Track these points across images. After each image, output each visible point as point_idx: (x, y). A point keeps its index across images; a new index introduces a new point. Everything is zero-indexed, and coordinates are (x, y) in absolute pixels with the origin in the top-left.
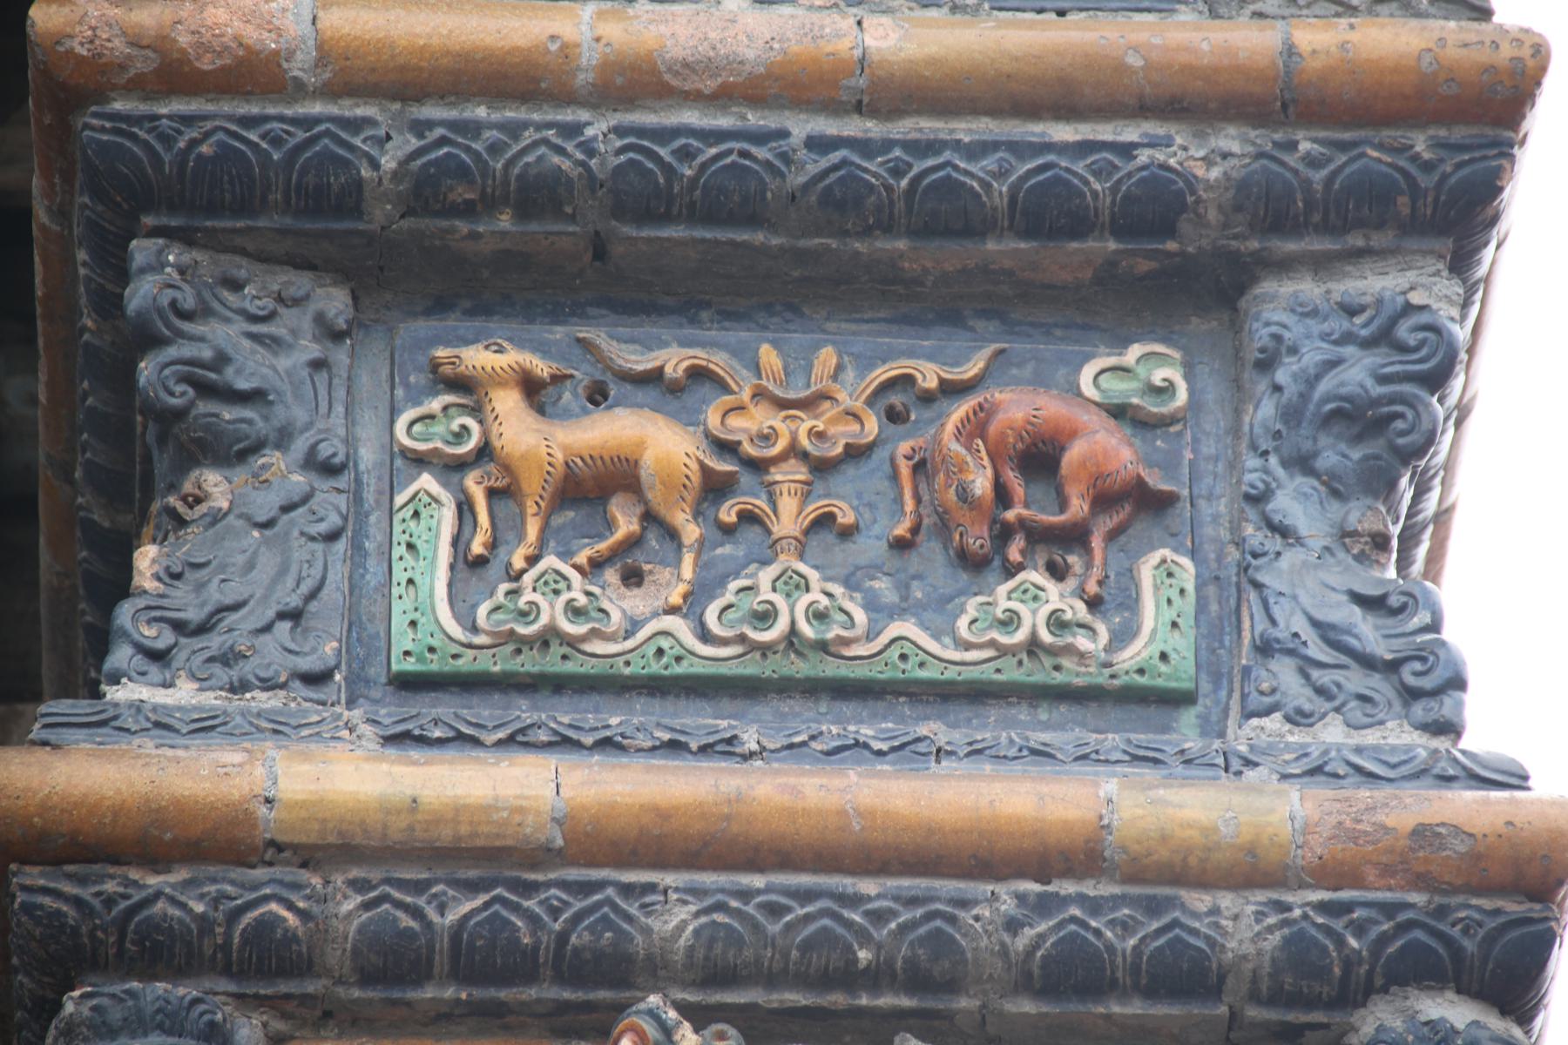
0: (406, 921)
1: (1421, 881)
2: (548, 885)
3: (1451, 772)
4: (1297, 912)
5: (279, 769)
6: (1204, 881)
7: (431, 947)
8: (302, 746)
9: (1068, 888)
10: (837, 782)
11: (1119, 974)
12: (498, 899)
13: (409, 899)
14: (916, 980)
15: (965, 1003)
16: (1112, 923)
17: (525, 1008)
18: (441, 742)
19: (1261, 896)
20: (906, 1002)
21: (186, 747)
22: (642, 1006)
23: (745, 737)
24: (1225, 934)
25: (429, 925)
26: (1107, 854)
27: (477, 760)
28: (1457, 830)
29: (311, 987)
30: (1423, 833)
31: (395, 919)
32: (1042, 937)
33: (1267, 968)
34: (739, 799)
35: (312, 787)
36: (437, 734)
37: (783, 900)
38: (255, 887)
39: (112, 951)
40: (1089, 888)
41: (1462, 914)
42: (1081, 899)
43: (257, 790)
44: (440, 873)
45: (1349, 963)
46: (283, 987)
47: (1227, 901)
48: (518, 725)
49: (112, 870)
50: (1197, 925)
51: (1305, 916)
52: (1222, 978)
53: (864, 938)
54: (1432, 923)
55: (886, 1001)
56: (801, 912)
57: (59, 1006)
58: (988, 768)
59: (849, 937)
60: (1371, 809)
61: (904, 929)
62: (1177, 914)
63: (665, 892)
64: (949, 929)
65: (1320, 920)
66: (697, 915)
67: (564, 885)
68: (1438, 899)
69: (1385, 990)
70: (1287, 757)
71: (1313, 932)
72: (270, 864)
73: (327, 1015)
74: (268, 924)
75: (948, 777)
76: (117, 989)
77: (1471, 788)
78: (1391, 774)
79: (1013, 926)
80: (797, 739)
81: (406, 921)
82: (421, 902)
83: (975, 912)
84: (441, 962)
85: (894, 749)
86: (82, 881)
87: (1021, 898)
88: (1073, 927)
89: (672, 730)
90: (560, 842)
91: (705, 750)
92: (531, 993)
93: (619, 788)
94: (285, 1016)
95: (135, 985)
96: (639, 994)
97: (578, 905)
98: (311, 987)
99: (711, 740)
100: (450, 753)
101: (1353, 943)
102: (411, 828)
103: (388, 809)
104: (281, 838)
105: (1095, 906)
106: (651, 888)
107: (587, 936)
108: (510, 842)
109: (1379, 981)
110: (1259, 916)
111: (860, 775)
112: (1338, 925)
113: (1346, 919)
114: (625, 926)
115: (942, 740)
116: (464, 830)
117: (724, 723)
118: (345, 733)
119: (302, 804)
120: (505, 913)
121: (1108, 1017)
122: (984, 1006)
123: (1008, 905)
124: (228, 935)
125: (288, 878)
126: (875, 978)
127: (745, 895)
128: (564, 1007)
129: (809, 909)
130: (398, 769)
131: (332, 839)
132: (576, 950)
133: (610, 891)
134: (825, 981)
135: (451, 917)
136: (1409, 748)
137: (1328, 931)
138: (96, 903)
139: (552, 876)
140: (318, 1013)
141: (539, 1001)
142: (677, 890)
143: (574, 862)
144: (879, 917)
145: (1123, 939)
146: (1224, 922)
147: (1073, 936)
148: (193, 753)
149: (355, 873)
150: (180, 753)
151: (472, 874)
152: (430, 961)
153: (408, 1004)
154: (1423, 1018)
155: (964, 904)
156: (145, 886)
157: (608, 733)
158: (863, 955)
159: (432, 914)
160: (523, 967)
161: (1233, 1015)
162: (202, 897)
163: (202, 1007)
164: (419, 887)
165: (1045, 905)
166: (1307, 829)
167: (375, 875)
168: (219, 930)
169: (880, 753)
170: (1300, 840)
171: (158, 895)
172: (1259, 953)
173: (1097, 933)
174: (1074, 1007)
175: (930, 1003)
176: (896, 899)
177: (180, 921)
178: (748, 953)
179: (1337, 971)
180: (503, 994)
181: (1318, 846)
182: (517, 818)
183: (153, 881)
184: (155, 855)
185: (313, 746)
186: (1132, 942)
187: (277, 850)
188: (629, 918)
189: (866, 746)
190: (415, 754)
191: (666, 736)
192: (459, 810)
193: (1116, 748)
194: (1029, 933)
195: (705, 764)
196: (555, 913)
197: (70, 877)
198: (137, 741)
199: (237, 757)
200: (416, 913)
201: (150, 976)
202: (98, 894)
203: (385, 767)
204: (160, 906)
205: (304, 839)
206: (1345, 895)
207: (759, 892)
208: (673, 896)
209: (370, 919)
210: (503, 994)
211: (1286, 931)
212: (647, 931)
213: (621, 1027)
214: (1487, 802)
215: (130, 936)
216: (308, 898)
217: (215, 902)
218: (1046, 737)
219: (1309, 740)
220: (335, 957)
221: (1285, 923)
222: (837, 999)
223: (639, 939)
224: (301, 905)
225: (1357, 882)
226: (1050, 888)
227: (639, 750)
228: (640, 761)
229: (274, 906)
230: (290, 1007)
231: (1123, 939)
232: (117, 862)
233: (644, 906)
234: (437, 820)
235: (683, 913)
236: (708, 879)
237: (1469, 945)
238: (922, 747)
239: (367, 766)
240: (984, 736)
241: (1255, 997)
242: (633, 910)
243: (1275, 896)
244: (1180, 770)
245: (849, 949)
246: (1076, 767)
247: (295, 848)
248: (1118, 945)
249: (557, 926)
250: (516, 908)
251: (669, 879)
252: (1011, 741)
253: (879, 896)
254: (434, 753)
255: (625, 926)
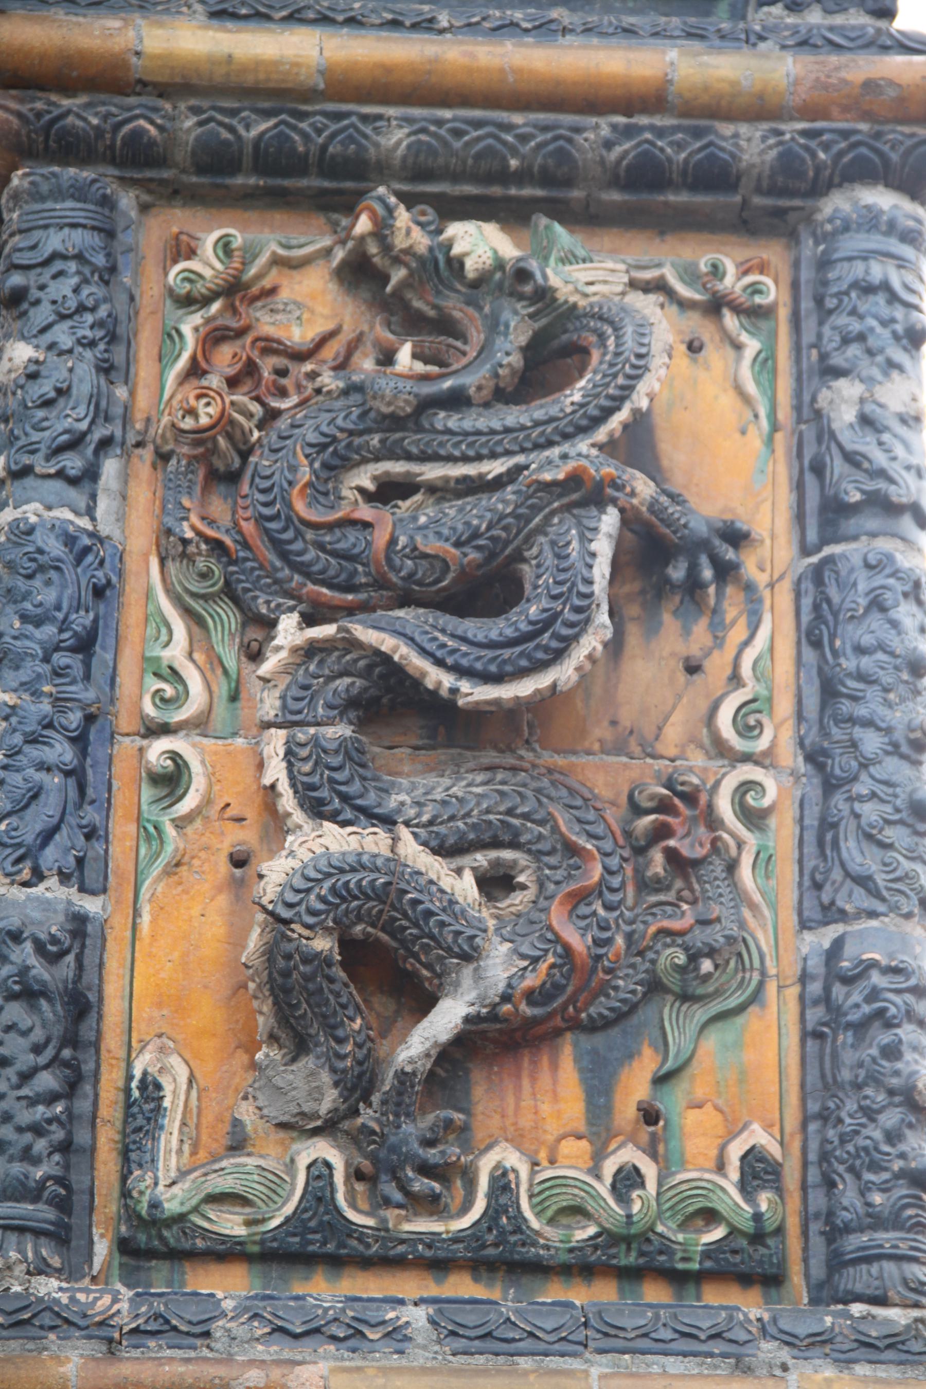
0: (225, 135)
1: (866, 116)
2: (315, 113)
3: (889, 43)
4: (788, 137)
5: (144, 32)
6: (729, 117)
7: (241, 152)
8: (157, 17)
9: (644, 120)
10: (499, 50)
11: (674, 176)
12: (283, 122)
13: (227, 120)
14: (546, 179)
15: (576, 194)
16: (671, 144)
17: (299, 192)
18: (246, 17)
19: (765, 126)
20: (539, 193)
21: (85, 16)
22: (374, 194)
23: (440, 18)
24: (741, 149)
25: (239, 137)
26: (670, 98)
27: (270, 30)
28: (891, 83)
29: (166, 174)
30: (870, 85)
31: (218, 134)
32: (626, 153)
33: (767, 172)
34: (436, 60)
35: (165, 45)
36: (244, 11)
37: (463, 126)
38: (130, 109)
39: (41, 147)
40: (659, 121)
41: (891, 137)
42: (652, 128)
43: (130, 46)
44: (246, 104)
45: (818, 169)
46: (149, 174)
47: (744, 129)
48: (295, 7)
49: (40, 94)
50: (724, 144)
51: (793, 139)
52: (738, 178)
53: (514, 152)
54: (871, 142)
55: (527, 192)
56: (475, 134)
57: (8, 180)
58: (595, 41)
59: (504, 150)
60: (837, 69)
61: (540, 146)
62: (712, 137)
63: (389, 120)
64: (568, 147)
65: (802, 141)
66: (409, 135)
67: (325, 114)
68: (877, 127)
69: (840, 185)
70: (786, 33)
71: (797, 149)
72: (139, 94)
73: (176, 192)
74: (138, 134)
75: (570, 47)
76: (45, 170)
77: (900, 53)
78: (851, 45)
79: (608, 145)
80: (474, 20)
81: (225, 135)
82: (234, 122)
83: (585, 135)
84: (247, 161)
85: (535, 28)
86: (22, 101)
87: (614, 127)
88: (646, 146)
89: (393, 12)
90: (322, 86)
91: (415, 26)
92: (304, 183)
93: (360, 51)
94: (150, 192)
95: (56, 169)
96: (372, 185)
97: (334, 127)
98: (166, 174)
99: (419, 19)
100: (252, 25)
101: (822, 155)
102: (228, 74)
103: (213, 61)
104: (146, 78)
105: (660, 132)
106: (379, 117)
107: (339, 148)
108: (290, 85)
109: (837, 180)
110: (764, 139)
111: (514, 45)
112: (813, 144)
113: (818, 140)
114: (364, 141)
115: (566, 21)
116: (262, 76)
117: (426, 8)
118: (185, 9)
119: (159, 57)
120: (287, 131)
121: (666, 204)
122: (589, 195)
123: (605, 132)
124: (113, 139)
125: (150, 104)
126: (522, 177)
127: (440, 123)
128: (323, 192)
129: (480, 132)
130: (221, 36)
131: (178, 80)
132: (333, 157)
133: (354, 119)
134: (489, 179)
135: (254, 133)
136: (863, 27)
137: (807, 148)
138: (31, 116)
139: (318, 107)
140: (170, 190)
141: (309, 188)
142: (396, 118)
143: (331, 99)
144: (524, 139)
145: (677, 154)
146: (742, 143)
147: (645, 153)
148: (89, 19)
149: (193, 102)
150: (81, 19)
151: (266, 105)
152: (240, 160)
153: (227, 187)
154: (863, 203)
155: (578, 130)
156: (59, 106)
157: (353, 14)
158: (514, 163)
159: (241, 130)
160: (297, 165)
161: (745, 203)
162: (96, 114)
163: (98, 185)
164: (233, 113)
165: (629, 132)
166: (797, 82)
167: (205, 104)
168: (108, 136)
169: (526, 30)
170: (792, 89)
171: (69, 112)
172: (763, 162)
173: (662, 150)
174: (645, 197)
175: (555, 193)
176: (535, 126)
177: (84, 130)
178: (441, 161)
179: (811, 174)
180: (287, 183)
181: (803, 94)
182: (295, 70)
183: (66, 102)
184: (68, 88)
185: (165, 17)
186: (683, 155)
187: (143, 86)
188: (366, 136)
189: (517, 25)
190: (229, 25)
191: (389, 16)
192: (258, 64)
193: (676, 28)
194: (618, 150)
195: (415, 36)
196: (319, 132)
197: (14, 98)
198: (53, 10)
199: (117, 24)
200: (231, 129)
201: (65, 163)
202: (32, 110)
203: (211, 33)
204: (70, 119)
205: (160, 79)
206: (819, 125)
207: (448, 121)
208: (394, 123)
209: (203, 133)
210: (287, 183)
211: (781, 148)
212: (377, 145)
213: (361, 206)
214: (910, 63)
215: (52, 137)
216: (163, 117)
217: (106, 117)
218: (632, 20)
219: (799, 21)
220: (181, 155)
221: (780, 143)
222: (496, 190)
223: (372, 150)
224: (159, 121)
225: (826, 117)
226: (633, 120)
227: (373, 25)
228: (374, 33)
229: (142, 122)
230: (153, 186)
231: (678, 153)
232: (42, 89)
233: (375, 129)
234: (243, 69)
235: (399, 134)
236: (417, 112)
237: (895, 157)
238: (553, 26)
239: (200, 33)
240: (593, 19)
241: (759, 190)
242: (368, 131)
243: (774, 125)
244: (717, 42)
245: (504, 160)
246: (652, 41)
247: (155, 85)
248: (675, 158)
249: (320, 140)
250: (294, 128)
251: (391, 111)
252: (610, 23)
253: (525, 125)
254: (241, 24)
255: (364, 141)
